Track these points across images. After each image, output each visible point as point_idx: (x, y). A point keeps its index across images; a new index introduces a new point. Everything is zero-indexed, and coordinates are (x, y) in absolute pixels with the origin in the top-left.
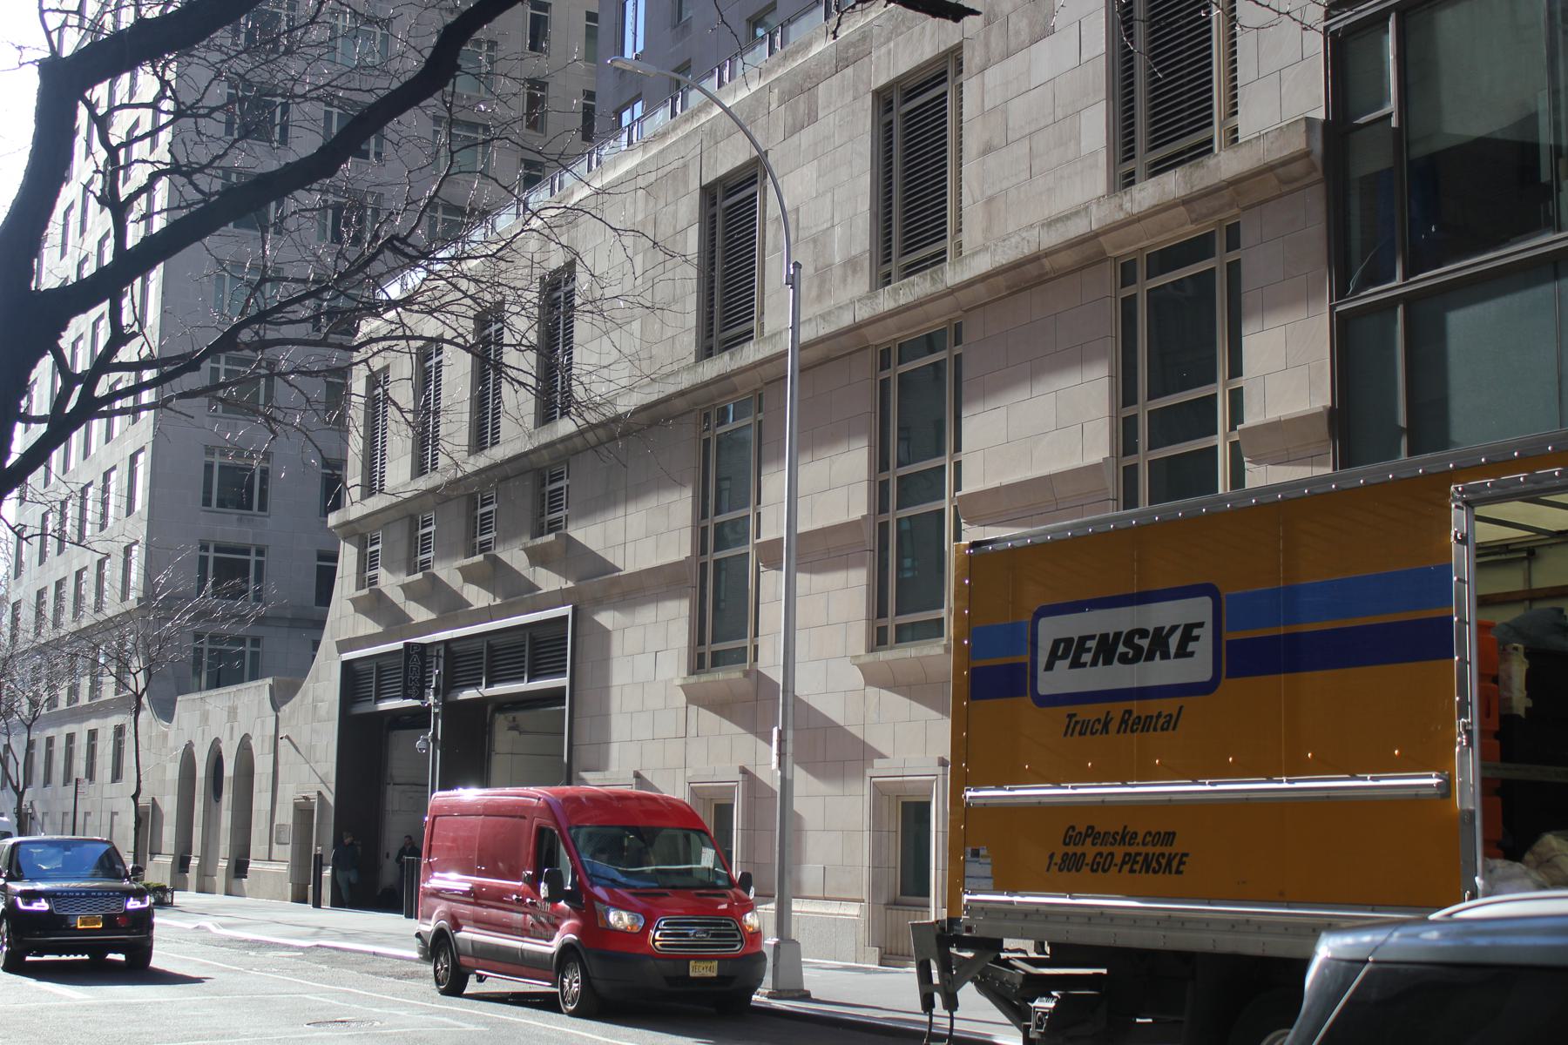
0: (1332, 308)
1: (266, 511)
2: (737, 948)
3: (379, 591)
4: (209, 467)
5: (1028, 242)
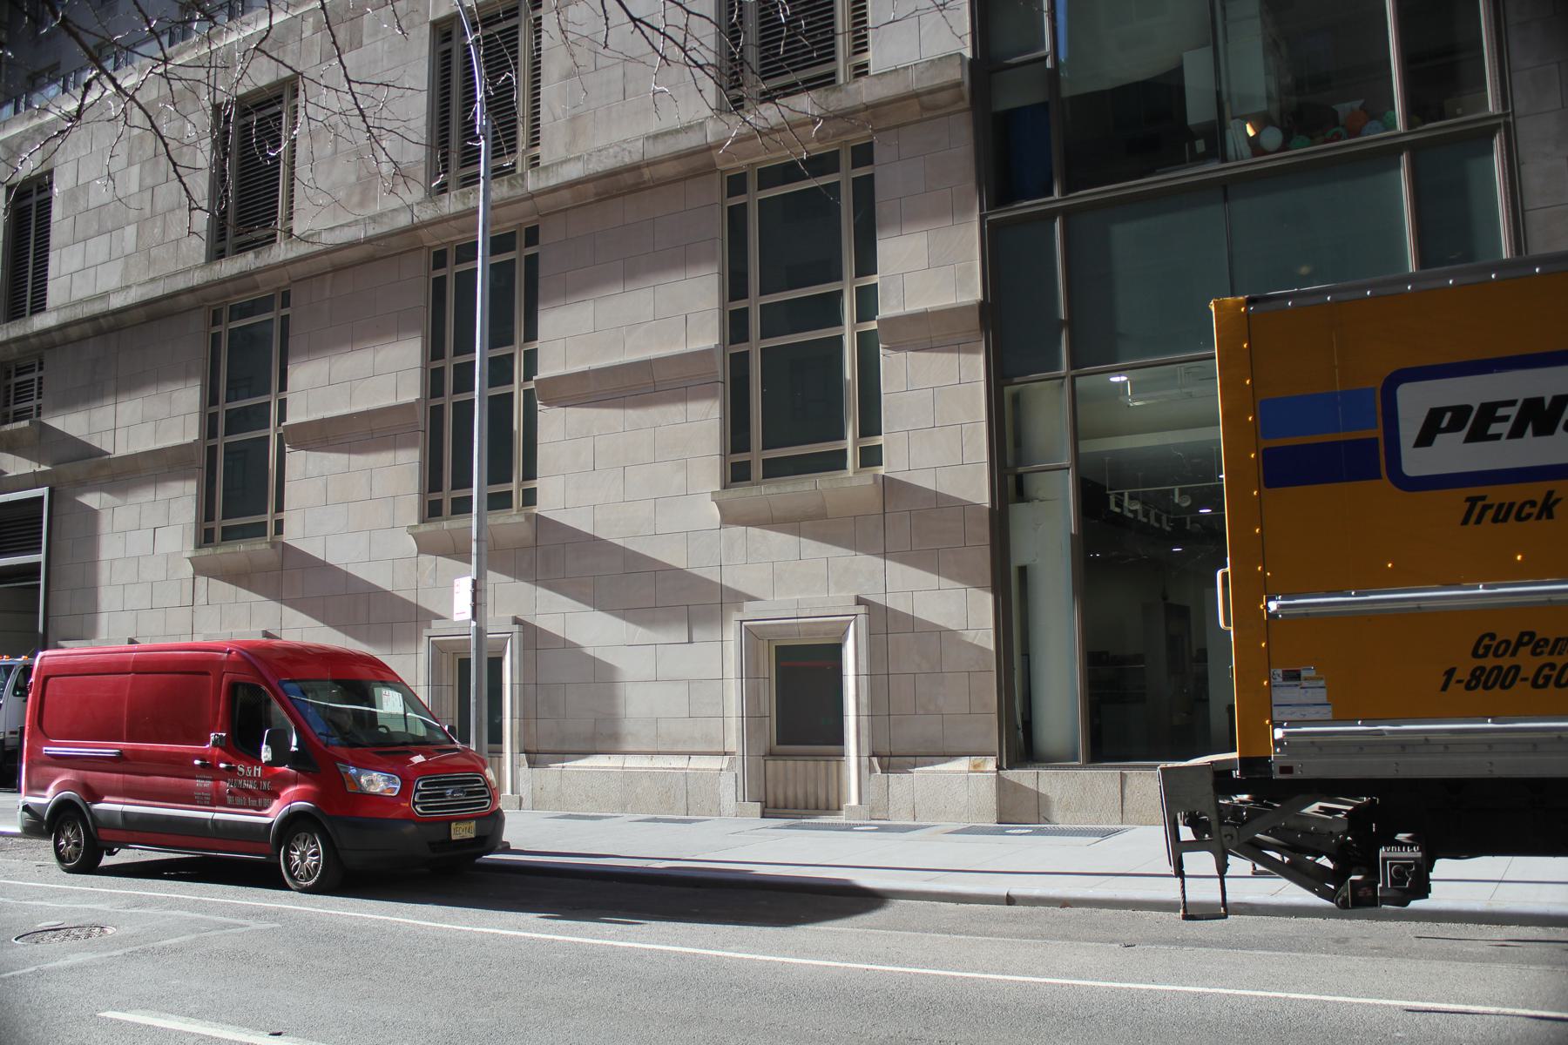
0: (982, 218)
2: (488, 805)
5: (630, 152)
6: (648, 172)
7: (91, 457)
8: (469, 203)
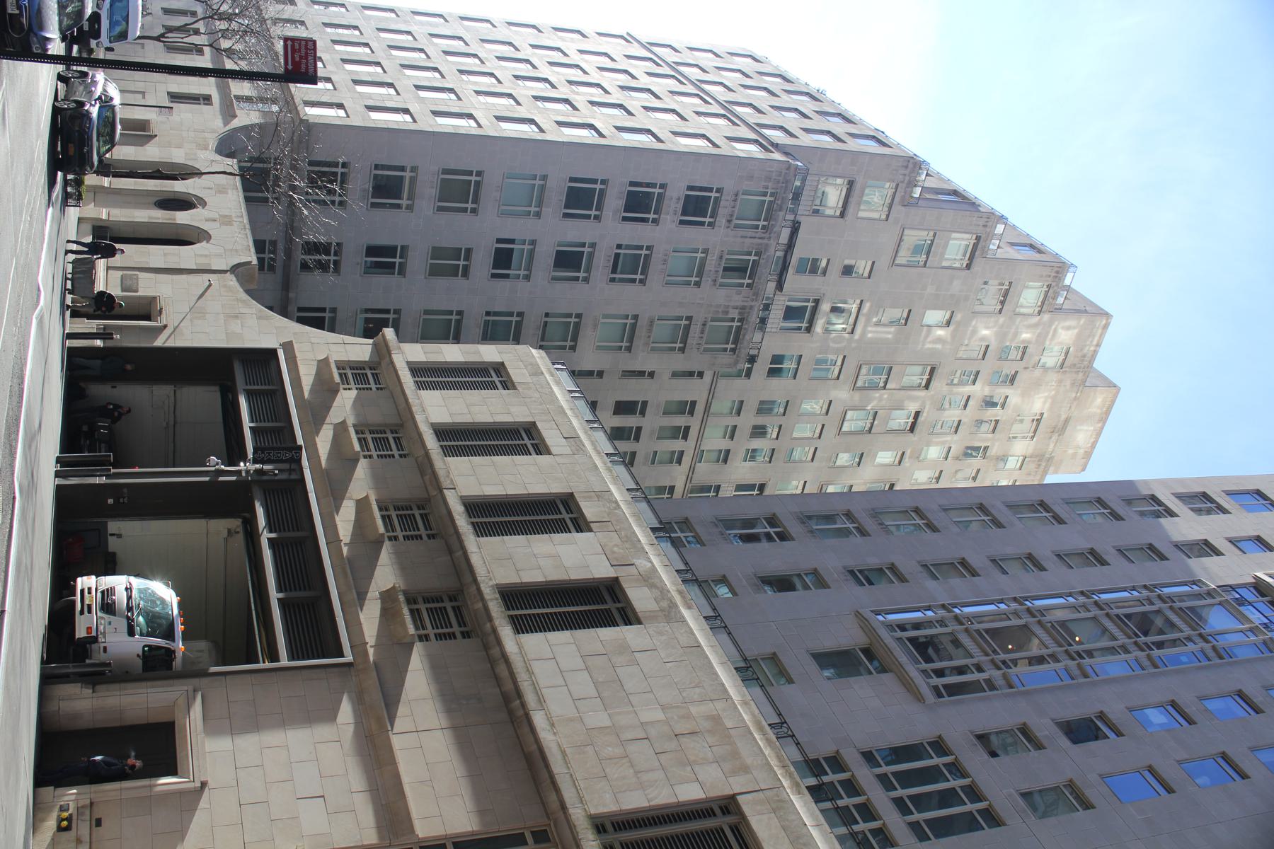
1: (371, 207)
3: (337, 391)
4: (402, 169)
7: (387, 705)
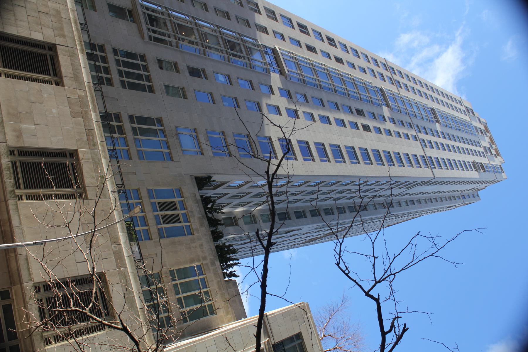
6: (13, 255)
8: (5, 171)
